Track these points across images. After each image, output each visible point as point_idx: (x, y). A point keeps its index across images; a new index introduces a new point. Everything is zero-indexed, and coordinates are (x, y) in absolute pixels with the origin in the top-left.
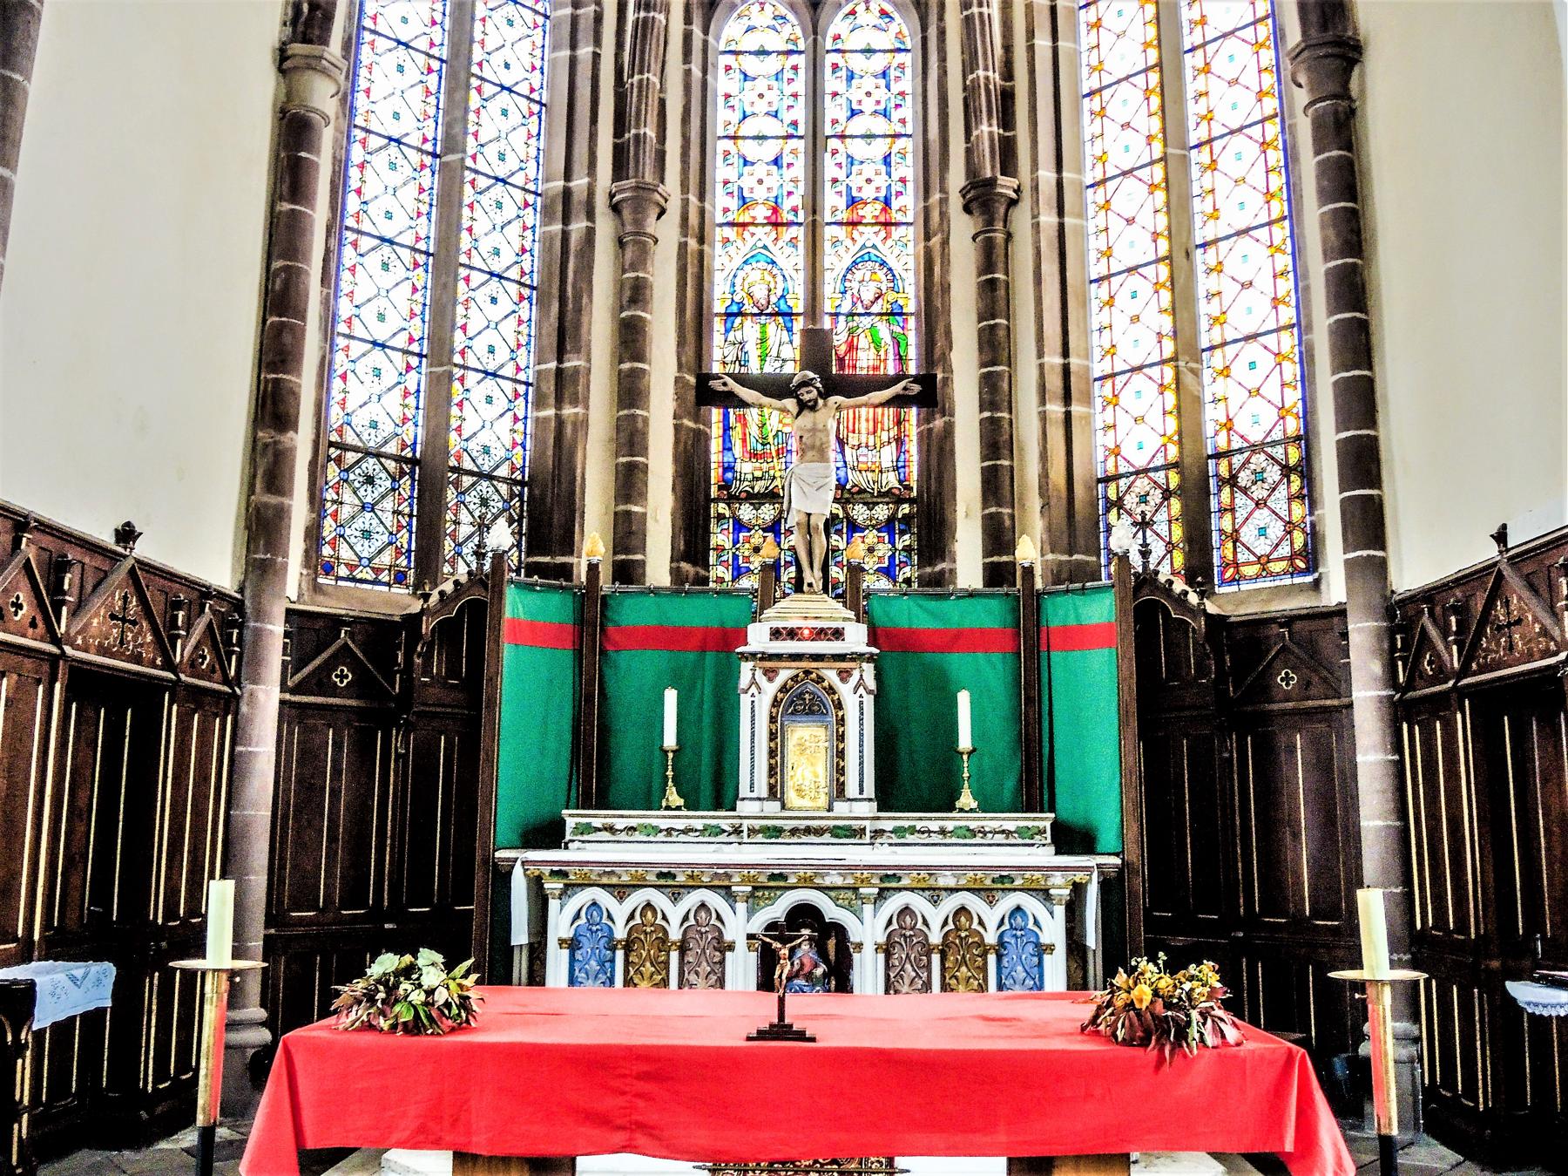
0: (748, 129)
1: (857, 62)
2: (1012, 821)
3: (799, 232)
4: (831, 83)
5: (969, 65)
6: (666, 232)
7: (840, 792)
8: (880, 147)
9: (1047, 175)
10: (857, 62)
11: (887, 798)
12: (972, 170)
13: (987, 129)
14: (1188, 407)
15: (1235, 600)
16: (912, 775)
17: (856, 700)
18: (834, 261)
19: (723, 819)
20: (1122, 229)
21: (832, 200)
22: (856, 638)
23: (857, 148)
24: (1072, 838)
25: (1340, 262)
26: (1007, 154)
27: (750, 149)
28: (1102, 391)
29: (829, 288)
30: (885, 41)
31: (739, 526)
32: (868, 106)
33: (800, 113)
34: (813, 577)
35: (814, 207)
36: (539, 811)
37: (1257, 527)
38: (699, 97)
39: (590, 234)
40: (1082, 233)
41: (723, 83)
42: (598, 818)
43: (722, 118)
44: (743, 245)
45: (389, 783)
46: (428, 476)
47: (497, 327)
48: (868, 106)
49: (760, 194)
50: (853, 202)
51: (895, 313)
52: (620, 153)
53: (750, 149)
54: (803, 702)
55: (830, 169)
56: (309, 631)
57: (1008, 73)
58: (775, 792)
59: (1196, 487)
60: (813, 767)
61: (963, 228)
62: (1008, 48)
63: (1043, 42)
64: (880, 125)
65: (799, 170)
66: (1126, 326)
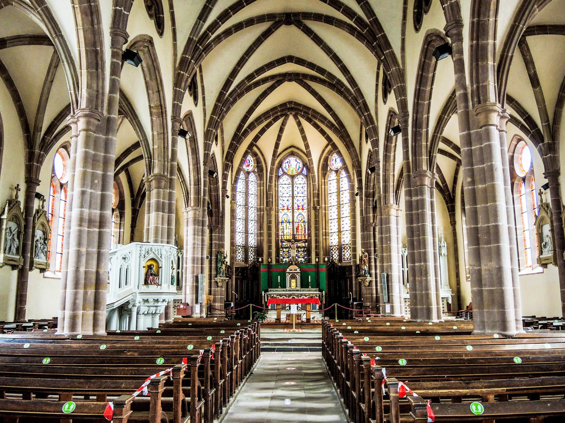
0: (284, 195)
1: (298, 185)
2: (314, 289)
3: (291, 211)
4: (295, 189)
5: (313, 191)
6: (273, 213)
7: (297, 286)
8: (302, 198)
9: (323, 206)
10: (298, 185)
11: (302, 287)
12: (314, 205)
13: (316, 199)
14: (340, 238)
15: (345, 263)
16: (304, 284)
17: (298, 277)
18: (296, 215)
19: (285, 289)
20: (333, 213)
21: (295, 206)
22: (298, 270)
23: (298, 198)
24: (320, 291)
25: (167, 420)
26: (318, 201)
27: (284, 198)
28: (330, 235)
29: (295, 219)
30: (303, 182)
31: (284, 252)
32: (300, 192)
33: (291, 193)
34: (294, 263)
35: (293, 208)
36: (266, 289)
37: (347, 254)
38: (277, 192)
39: (263, 214)
40: (328, 213)
41: (280, 189)
42: (272, 289)
43: (280, 194)
44: (283, 213)
45: (244, 286)
46: (246, 248)
47: (253, 227)
48: (300, 192)
49: (285, 205)
50: (298, 206)
51: (304, 222)
52: (267, 202)
53: (284, 198)
54: (293, 277)
55: (295, 201)
56: (237, 269)
57: (319, 191)
58: (290, 286)
59: (340, 248)
60: (293, 284)
61: (313, 212)
62: (319, 187)
63: (323, 187)
64: (302, 195)
65: (291, 201)
66: (333, 227)
